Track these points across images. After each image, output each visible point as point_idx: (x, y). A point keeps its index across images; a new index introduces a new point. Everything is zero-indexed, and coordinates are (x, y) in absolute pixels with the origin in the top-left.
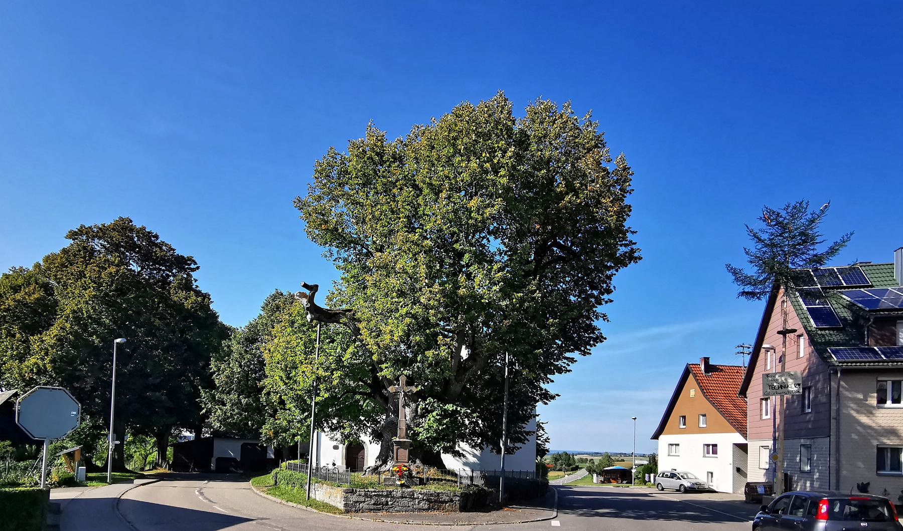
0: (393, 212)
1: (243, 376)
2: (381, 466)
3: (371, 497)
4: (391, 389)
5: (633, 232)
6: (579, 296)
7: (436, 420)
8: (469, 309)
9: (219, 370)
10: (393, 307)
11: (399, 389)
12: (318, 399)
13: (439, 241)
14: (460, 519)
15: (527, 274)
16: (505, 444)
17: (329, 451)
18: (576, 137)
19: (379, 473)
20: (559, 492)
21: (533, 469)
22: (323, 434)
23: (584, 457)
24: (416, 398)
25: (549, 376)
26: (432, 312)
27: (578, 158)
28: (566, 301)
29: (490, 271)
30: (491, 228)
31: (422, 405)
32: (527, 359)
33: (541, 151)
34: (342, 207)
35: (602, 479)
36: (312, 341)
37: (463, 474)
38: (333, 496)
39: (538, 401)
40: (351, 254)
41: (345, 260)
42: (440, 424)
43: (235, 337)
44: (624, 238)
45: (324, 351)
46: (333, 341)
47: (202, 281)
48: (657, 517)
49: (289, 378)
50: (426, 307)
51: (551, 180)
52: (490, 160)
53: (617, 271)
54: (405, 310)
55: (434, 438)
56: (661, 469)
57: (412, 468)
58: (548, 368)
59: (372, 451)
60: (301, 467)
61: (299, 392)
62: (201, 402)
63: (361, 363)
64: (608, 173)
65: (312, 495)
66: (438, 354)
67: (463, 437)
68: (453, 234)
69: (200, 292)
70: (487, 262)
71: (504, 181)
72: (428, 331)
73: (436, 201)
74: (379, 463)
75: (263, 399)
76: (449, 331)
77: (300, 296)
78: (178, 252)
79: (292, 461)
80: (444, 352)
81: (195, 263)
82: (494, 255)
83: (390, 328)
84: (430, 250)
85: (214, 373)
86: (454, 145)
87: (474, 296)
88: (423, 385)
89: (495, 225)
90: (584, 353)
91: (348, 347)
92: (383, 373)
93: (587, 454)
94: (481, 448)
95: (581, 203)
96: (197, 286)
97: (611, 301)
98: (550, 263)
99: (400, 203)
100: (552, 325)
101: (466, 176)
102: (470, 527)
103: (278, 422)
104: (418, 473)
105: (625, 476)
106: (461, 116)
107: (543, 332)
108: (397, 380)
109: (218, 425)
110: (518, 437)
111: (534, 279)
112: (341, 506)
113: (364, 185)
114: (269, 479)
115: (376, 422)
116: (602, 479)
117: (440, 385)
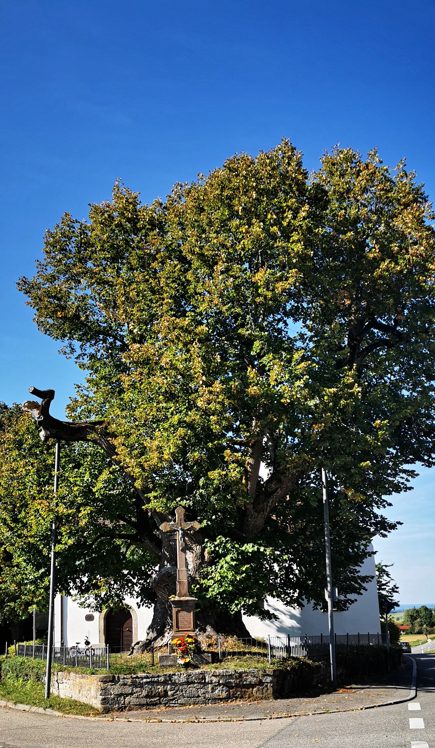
0: (153, 292)
2: (155, 639)
3: (141, 686)
4: (164, 527)
7: (231, 568)
10: (161, 415)
11: (176, 527)
12: (59, 548)
13: (219, 326)
14: (275, 710)
15: (340, 364)
16: (332, 595)
17: (78, 622)
19: (152, 650)
20: (420, 663)
21: (377, 630)
22: (69, 597)
25: (384, 497)
28: (397, 398)
29: (289, 361)
30: (288, 307)
31: (210, 547)
34: (85, 289)
37: (276, 643)
39: (374, 534)
40: (99, 349)
42: (237, 573)
45: (67, 479)
46: (78, 466)
49: (16, 520)
50: (206, 413)
51: (362, 245)
52: (277, 222)
57: (200, 638)
58: (383, 486)
59: (142, 617)
60: (38, 649)
61: (31, 540)
63: (120, 494)
65: (54, 690)
66: (226, 475)
67: (272, 590)
70: (285, 350)
71: (298, 247)
72: (210, 445)
74: (152, 635)
76: (241, 444)
77: (29, 407)
79: (24, 643)
80: (234, 472)
83: (157, 443)
86: (230, 207)
87: (269, 396)
88: (210, 520)
92: (150, 506)
94: (300, 605)
95: (401, 271)
98: (368, 349)
99: (163, 280)
100: (380, 428)
102: (289, 720)
104: (210, 645)
106: (236, 170)
107: (369, 438)
108: (173, 514)
110: (350, 585)
111: (350, 370)
112: (97, 703)
113: (114, 260)
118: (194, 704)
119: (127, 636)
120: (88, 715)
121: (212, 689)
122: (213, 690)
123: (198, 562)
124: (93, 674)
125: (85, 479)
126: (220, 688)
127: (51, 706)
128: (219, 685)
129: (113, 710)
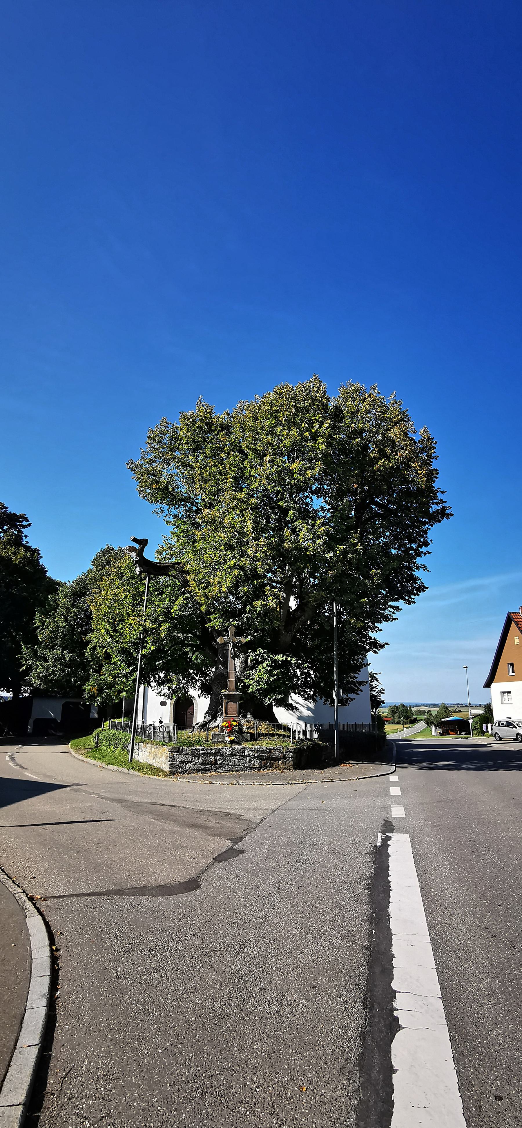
0: (221, 474)
1: (68, 631)
2: (210, 721)
3: (199, 756)
5: (443, 492)
6: (399, 549)
7: (266, 672)
8: (296, 561)
9: (43, 624)
10: (221, 560)
11: (228, 640)
12: (145, 651)
14: (294, 778)
15: (348, 529)
16: (338, 694)
17: (155, 707)
18: (384, 413)
19: (208, 729)
20: (398, 746)
21: (369, 721)
23: (422, 709)
24: (245, 649)
26: (259, 563)
27: (386, 430)
28: (387, 554)
29: (313, 525)
30: (314, 488)
31: (252, 656)
32: (354, 608)
33: (355, 423)
34: (173, 469)
35: (440, 730)
36: (141, 594)
37: (297, 728)
38: (154, 755)
39: (368, 651)
40: (181, 511)
41: (176, 516)
42: (271, 676)
43: (63, 591)
44: (435, 497)
45: (152, 603)
46: (161, 593)
47: (32, 538)
48: (496, 768)
49: (115, 631)
50: (254, 560)
51: (366, 448)
53: (432, 526)
54: (232, 562)
55: (265, 689)
56: (496, 718)
57: (242, 722)
58: (376, 617)
59: (202, 705)
60: (126, 725)
62: (22, 658)
63: (190, 615)
64: (415, 442)
66: (266, 604)
67: (295, 689)
68: (277, 493)
69: (30, 547)
70: (310, 517)
71: (322, 447)
72: (255, 582)
73: (261, 464)
74: (208, 719)
75: (88, 653)
78: (11, 510)
79: (116, 720)
80: (271, 603)
81: (27, 520)
82: (316, 512)
84: (256, 508)
85: (38, 627)
86: (276, 418)
89: (317, 485)
90: (409, 602)
91: (177, 599)
92: (211, 624)
93: (424, 705)
94: (314, 700)
95: (392, 467)
96: (27, 542)
97: (429, 553)
98: (369, 519)
100: (376, 575)
101: (287, 442)
103: (103, 677)
105: (462, 727)
109: (38, 682)
110: (351, 687)
112: (166, 768)
114: (90, 740)
115: (204, 674)
116: (440, 730)
117: (269, 636)
118: (236, 771)
119: (189, 718)
120: (159, 776)
121: (250, 760)
122: (250, 761)
123: (243, 666)
124: (164, 745)
125: (166, 603)
126: (255, 760)
127: (133, 768)
128: (255, 757)
129: (177, 773)
